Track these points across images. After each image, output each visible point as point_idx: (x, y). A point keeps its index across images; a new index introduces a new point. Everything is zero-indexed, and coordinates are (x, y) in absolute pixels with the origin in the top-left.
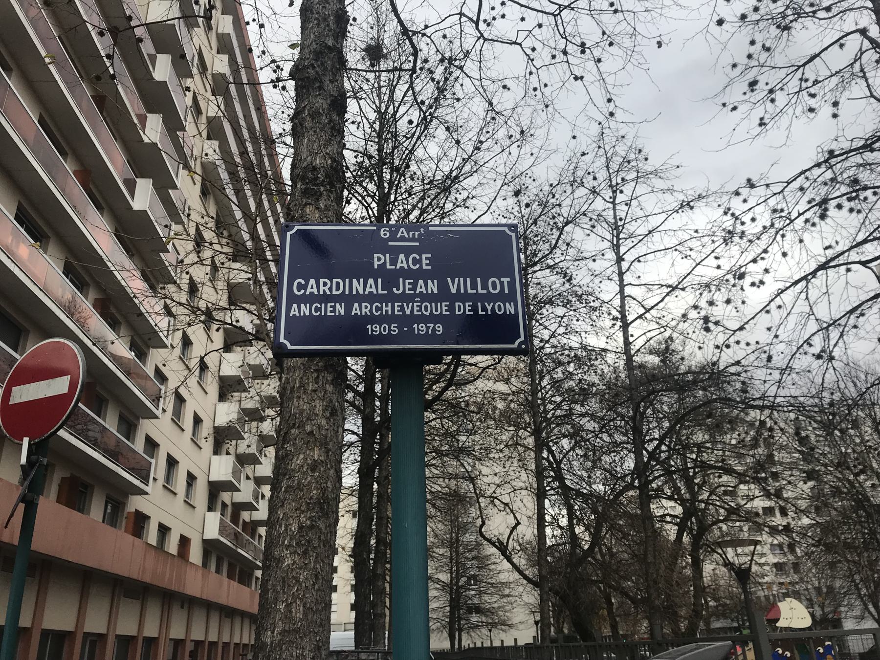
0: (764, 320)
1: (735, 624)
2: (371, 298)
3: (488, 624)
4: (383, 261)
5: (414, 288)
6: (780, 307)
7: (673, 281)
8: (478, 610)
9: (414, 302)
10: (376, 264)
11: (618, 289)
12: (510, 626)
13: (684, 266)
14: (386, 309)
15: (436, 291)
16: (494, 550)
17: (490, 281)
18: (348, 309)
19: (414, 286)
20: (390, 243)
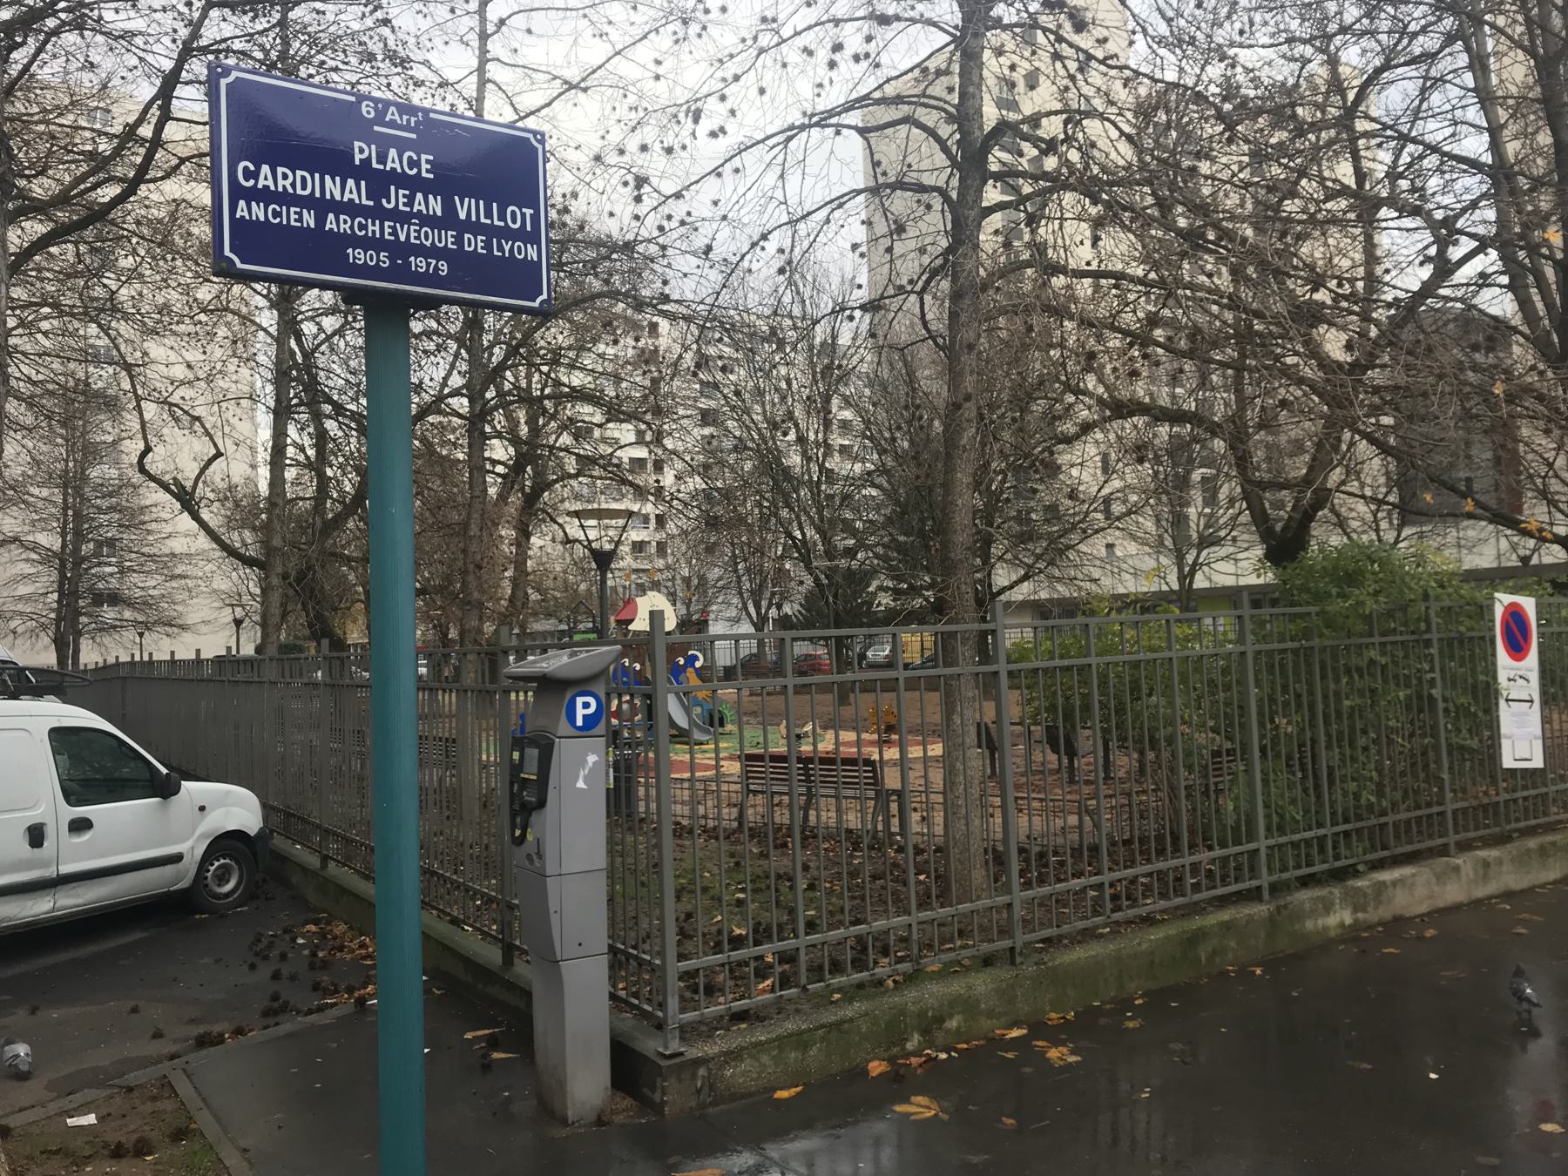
0: (711, 187)
1: (564, 627)
2: (351, 209)
3: (136, 623)
4: (366, 154)
5: (410, 203)
6: (737, 171)
7: (573, 75)
8: (114, 599)
9: (410, 224)
10: (358, 158)
11: (475, 63)
12: (183, 627)
13: (595, 52)
14: (373, 228)
15: (439, 213)
16: (162, 496)
17: (510, 209)
18: (320, 220)
19: (410, 202)
20: (376, 128)
